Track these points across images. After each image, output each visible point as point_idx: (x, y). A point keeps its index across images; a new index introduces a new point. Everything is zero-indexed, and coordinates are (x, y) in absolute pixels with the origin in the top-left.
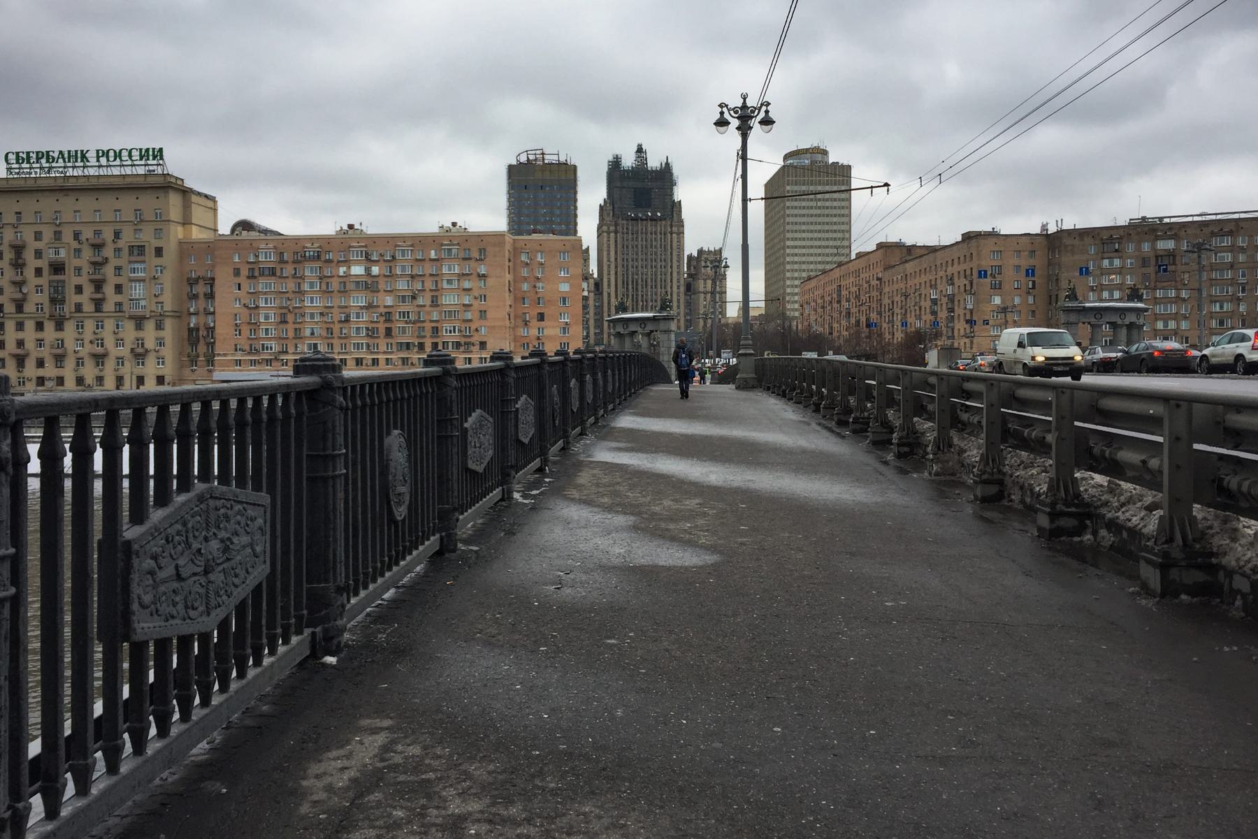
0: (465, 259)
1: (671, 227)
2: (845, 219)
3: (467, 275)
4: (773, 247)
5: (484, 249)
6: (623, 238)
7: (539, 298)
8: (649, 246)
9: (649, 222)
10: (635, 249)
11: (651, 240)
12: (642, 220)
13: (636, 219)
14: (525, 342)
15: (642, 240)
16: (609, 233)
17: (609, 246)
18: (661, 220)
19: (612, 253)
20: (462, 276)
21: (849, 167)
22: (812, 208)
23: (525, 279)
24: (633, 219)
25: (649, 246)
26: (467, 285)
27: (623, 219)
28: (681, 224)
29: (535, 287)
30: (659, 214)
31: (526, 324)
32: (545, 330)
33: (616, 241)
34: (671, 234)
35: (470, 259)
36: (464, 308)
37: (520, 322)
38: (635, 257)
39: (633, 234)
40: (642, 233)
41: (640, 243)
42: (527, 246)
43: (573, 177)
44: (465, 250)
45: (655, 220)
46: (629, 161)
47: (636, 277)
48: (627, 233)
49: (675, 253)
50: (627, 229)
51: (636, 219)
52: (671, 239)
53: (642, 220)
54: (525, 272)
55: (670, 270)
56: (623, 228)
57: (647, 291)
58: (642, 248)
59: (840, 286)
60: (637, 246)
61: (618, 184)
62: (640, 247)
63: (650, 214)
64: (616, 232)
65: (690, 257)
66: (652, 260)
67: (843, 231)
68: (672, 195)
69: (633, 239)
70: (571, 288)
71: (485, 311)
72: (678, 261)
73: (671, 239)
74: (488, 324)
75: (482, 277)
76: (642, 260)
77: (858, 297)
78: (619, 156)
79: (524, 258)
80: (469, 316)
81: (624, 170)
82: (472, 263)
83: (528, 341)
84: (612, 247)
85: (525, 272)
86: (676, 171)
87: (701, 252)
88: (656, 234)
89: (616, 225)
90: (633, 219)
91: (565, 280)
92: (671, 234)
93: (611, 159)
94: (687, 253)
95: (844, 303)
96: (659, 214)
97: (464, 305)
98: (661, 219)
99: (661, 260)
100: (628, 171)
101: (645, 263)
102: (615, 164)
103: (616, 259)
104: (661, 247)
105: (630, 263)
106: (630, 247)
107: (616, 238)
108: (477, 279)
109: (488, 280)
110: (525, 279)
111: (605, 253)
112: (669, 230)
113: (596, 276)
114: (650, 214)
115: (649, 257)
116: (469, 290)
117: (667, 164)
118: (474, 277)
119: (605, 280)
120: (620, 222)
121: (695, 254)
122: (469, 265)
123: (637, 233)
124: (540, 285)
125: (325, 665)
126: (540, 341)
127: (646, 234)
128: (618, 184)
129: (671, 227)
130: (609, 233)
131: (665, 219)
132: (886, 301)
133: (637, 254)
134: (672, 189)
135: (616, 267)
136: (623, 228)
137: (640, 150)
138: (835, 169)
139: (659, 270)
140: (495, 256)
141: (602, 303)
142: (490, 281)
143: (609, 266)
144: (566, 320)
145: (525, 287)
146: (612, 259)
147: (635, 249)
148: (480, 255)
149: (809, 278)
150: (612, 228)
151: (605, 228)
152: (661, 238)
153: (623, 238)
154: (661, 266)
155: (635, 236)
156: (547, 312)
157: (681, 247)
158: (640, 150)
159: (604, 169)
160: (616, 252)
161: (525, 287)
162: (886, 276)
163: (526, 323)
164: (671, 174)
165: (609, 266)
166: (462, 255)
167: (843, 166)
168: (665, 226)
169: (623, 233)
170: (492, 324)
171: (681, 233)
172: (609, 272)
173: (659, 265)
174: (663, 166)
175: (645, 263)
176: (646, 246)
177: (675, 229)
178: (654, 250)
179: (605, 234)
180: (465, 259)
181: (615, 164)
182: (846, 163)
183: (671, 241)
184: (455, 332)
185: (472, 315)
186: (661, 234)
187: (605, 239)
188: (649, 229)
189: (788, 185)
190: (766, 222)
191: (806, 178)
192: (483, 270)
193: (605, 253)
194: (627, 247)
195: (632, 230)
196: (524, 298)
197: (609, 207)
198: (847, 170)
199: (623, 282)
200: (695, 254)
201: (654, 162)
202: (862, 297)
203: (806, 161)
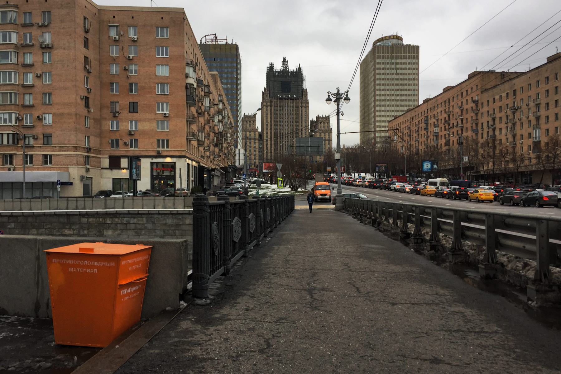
0: (25, 26)
1: (302, 103)
2: (416, 82)
3: (27, 46)
4: (364, 109)
5: (49, 12)
6: (275, 109)
7: (131, 84)
8: (289, 114)
9: (289, 101)
10: (282, 116)
11: (291, 111)
12: (285, 99)
13: (282, 99)
14: (114, 138)
15: (285, 111)
16: (267, 106)
17: (267, 114)
18: (296, 99)
19: (269, 118)
20: (21, 48)
21: (418, 47)
22: (393, 74)
23: (114, 60)
24: (280, 99)
25: (289, 114)
26: (28, 59)
27: (275, 99)
28: (307, 102)
29: (126, 70)
30: (295, 96)
31: (115, 116)
32: (138, 123)
33: (271, 111)
34: (302, 108)
35: (31, 25)
36: (21, 90)
37: (106, 113)
38: (281, 120)
39: (280, 107)
40: (285, 107)
41: (284, 112)
42: (117, 18)
43: (235, 53)
44: (25, 13)
45: (293, 99)
46: (278, 67)
47: (282, 131)
48: (277, 107)
49: (303, 119)
50: (277, 104)
51: (282, 99)
52: (302, 110)
53: (285, 99)
54: (114, 52)
55: (301, 124)
56: (275, 103)
57: (288, 139)
58: (285, 115)
59: (427, 116)
60: (282, 114)
61: (272, 79)
62: (284, 114)
63: (290, 96)
64: (271, 106)
65: (312, 121)
66: (291, 122)
67: (414, 90)
68: (302, 85)
69: (280, 110)
70: (170, 73)
71: (50, 94)
72: (305, 123)
73: (302, 110)
74: (54, 111)
75: (47, 48)
76: (285, 122)
77: (447, 122)
78: (273, 63)
79: (113, 33)
80: (28, 100)
81: (276, 72)
82: (35, 32)
83: (117, 136)
84: (269, 114)
85: (114, 52)
86: (304, 73)
87: (318, 117)
88: (293, 107)
89: (271, 102)
90: (280, 99)
91: (164, 62)
92: (302, 108)
93: (269, 66)
94: (310, 119)
95: (431, 128)
96: (295, 96)
97: (24, 86)
98: (296, 99)
99: (296, 122)
100: (278, 72)
101: (287, 123)
102: (271, 68)
103: (271, 121)
104: (296, 115)
105: (279, 123)
106: (279, 114)
107: (271, 110)
108: (40, 52)
109: (55, 52)
110: (114, 60)
111: (265, 118)
112: (301, 105)
113: (260, 130)
114: (290, 96)
115: (289, 120)
116: (31, 66)
117: (299, 68)
118: (36, 49)
119: (265, 133)
120: (273, 100)
121: (315, 119)
122: (30, 34)
123: (282, 107)
124: (133, 67)
125: (117, 348)
126: (133, 138)
127: (288, 107)
128: (272, 79)
129: (302, 103)
130: (267, 106)
131: (298, 99)
132: (484, 119)
133: (282, 118)
134: (302, 83)
135: (271, 126)
136: (275, 103)
137: (284, 61)
138: (409, 48)
139: (295, 127)
140: (62, 21)
141: (263, 146)
142: (57, 54)
143: (267, 125)
144: (165, 112)
145: (114, 69)
146: (269, 121)
147: (282, 116)
148: (44, 19)
149: (408, 111)
150: (269, 104)
151: (265, 104)
152: (296, 110)
153: (275, 109)
154: (296, 125)
155: (282, 108)
156: (142, 101)
157: (307, 115)
158: (284, 61)
159: (265, 71)
160: (271, 117)
161: (114, 69)
162: (485, 97)
163: (115, 115)
164: (302, 74)
165: (267, 125)
166: (21, 21)
167: (414, 46)
168: (298, 103)
169: (275, 107)
170: (60, 111)
171: (307, 107)
172: (267, 128)
173: (295, 124)
174: (297, 69)
175: (287, 123)
176: (287, 114)
177: (304, 105)
178: (292, 116)
179: (265, 107)
180: (25, 26)
181: (271, 68)
182: (416, 44)
183: (302, 112)
184: (11, 121)
185: (35, 99)
186: (296, 107)
187: (265, 110)
188: (289, 104)
189: (378, 58)
190: (360, 88)
191: (390, 54)
192: (47, 39)
193: (265, 118)
194: (277, 114)
195: (280, 105)
196: (112, 84)
197: (267, 92)
198: (417, 49)
199: (275, 134)
200: (315, 119)
201: (292, 67)
202: (452, 122)
203: (389, 43)
